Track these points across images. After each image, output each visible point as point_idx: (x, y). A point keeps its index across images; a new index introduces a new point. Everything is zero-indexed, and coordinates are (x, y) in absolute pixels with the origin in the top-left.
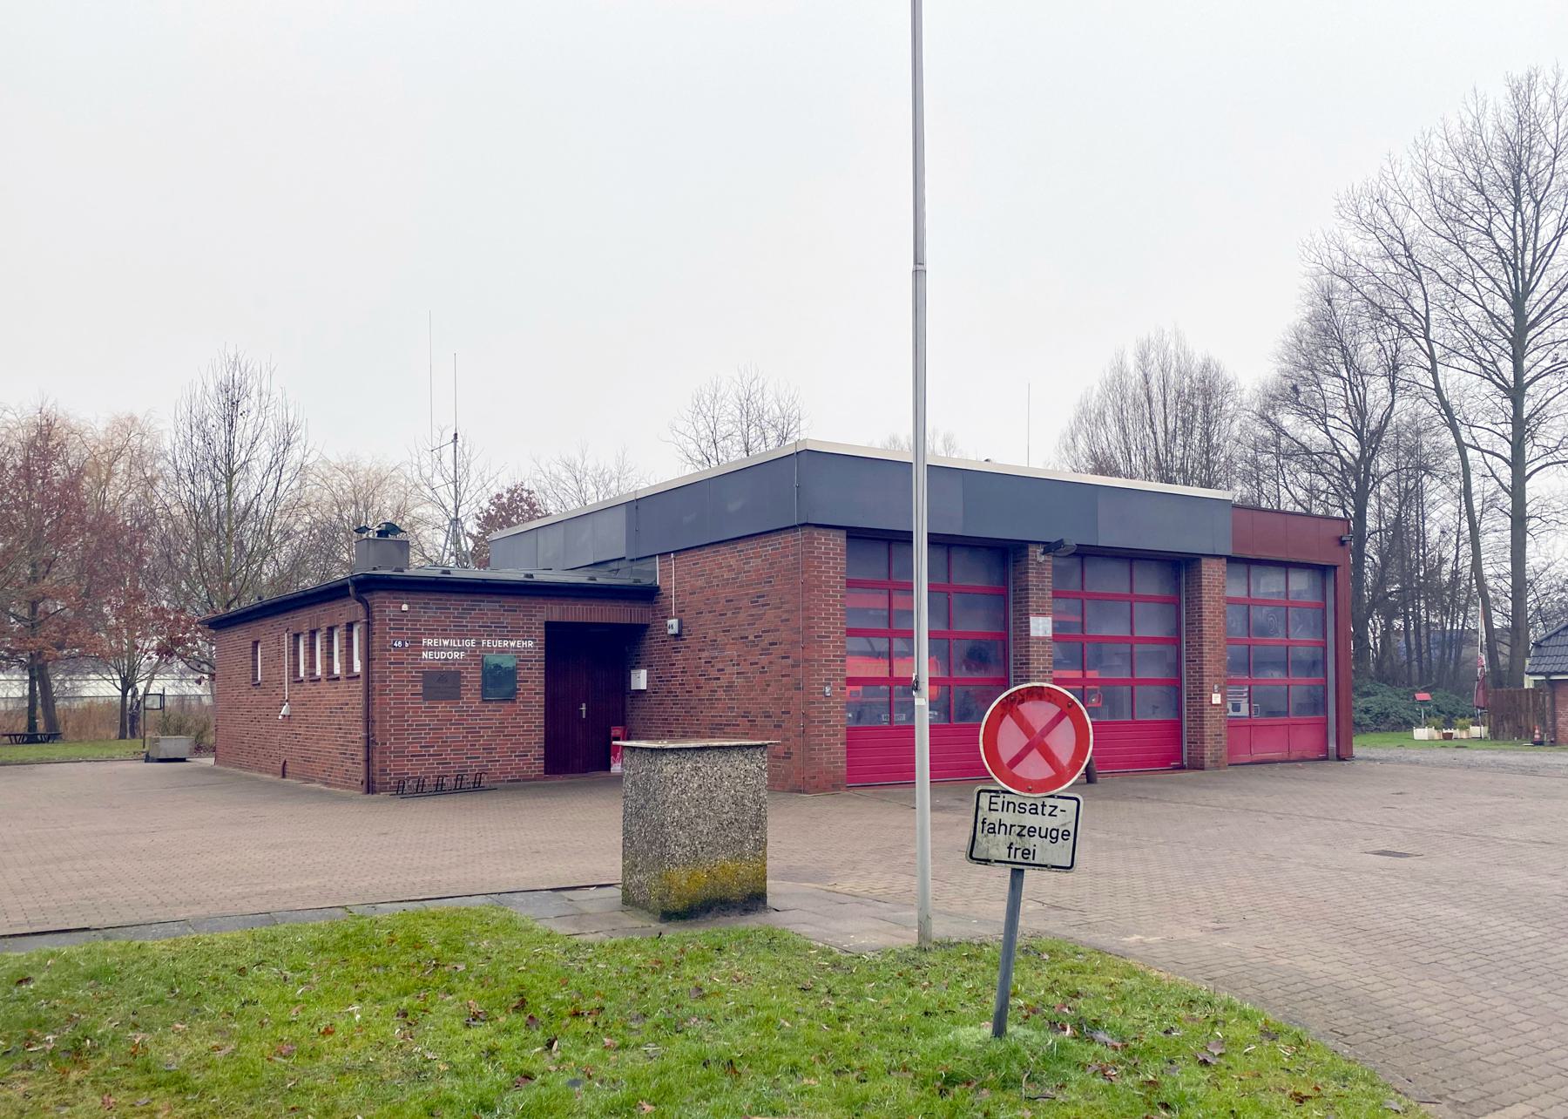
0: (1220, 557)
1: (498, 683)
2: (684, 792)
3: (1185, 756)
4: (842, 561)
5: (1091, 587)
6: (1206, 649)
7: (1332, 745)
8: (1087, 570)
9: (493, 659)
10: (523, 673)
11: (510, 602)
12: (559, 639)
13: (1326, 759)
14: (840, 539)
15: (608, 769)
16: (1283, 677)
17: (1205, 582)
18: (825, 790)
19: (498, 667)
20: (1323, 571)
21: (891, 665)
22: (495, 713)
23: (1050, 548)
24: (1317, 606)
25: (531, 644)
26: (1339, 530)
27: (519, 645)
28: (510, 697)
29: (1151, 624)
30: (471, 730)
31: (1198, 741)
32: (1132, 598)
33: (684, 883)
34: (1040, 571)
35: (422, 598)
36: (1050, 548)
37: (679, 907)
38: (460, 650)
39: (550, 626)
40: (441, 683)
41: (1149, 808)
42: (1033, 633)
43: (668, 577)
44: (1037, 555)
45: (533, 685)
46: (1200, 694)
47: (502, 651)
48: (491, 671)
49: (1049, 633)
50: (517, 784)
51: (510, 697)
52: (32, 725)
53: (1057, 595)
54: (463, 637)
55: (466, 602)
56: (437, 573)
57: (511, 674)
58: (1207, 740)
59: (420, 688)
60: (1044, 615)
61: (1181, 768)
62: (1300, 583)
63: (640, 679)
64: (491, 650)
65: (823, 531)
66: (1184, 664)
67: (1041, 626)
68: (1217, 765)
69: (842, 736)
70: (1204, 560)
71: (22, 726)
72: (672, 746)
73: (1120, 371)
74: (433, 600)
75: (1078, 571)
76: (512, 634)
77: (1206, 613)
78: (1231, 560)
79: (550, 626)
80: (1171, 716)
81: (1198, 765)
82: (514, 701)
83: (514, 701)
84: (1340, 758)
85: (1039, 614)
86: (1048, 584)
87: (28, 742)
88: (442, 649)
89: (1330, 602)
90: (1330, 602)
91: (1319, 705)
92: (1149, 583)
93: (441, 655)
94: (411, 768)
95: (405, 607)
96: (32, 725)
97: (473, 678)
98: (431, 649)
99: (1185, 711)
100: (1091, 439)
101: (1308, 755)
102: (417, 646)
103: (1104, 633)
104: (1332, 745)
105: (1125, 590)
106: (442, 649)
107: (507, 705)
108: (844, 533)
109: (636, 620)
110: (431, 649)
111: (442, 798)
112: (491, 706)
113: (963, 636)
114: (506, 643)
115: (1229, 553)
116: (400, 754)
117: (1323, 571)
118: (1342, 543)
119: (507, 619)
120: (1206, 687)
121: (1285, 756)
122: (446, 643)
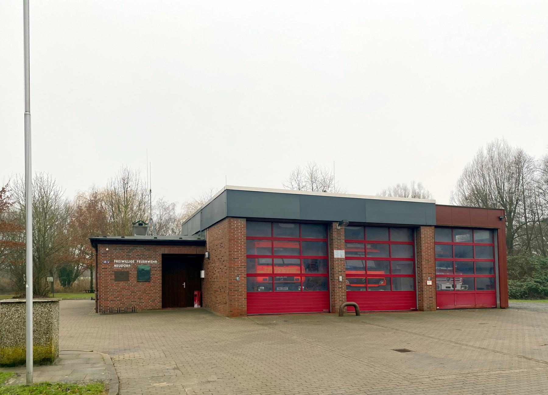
0: (431, 226)
1: (144, 275)
2: (11, 319)
3: (418, 306)
4: (244, 230)
5: (392, 239)
6: (423, 263)
7: (498, 302)
8: (391, 233)
9: (141, 267)
10: (153, 272)
11: (148, 247)
12: (166, 259)
13: (496, 308)
14: (244, 222)
15: (193, 306)
16: (452, 274)
17: (422, 236)
18: (237, 316)
19: (143, 270)
20: (493, 231)
21: (273, 269)
22: (143, 286)
23: (341, 223)
24: (490, 245)
25: (156, 262)
26: (499, 214)
27: (152, 262)
28: (148, 280)
29: (403, 253)
30: (133, 292)
31: (422, 300)
32: (390, 243)
33: (10, 353)
34: (338, 234)
35: (114, 246)
36: (341, 223)
37: (8, 362)
38: (128, 264)
39: (164, 256)
40: (122, 275)
41: (368, 326)
42: (335, 256)
43: (208, 237)
44: (336, 226)
45: (157, 277)
46: (421, 281)
47: (145, 264)
48: (140, 271)
49: (344, 257)
50: (150, 311)
51: (148, 280)
52: (92, 287)
53: (347, 241)
54: (129, 259)
55: (131, 247)
56: (178, 239)
57: (148, 273)
58: (425, 299)
59: (113, 277)
60: (340, 249)
61: (416, 310)
62: (483, 237)
63: (203, 274)
64: (141, 264)
65: (235, 219)
66: (416, 269)
67: (339, 254)
68: (430, 309)
69: (245, 296)
70: (422, 227)
71: (88, 287)
72: (12, 301)
73: (481, 155)
74: (118, 247)
75: (362, 234)
76: (149, 258)
77: (423, 248)
78: (436, 227)
79: (164, 256)
80: (412, 290)
81: (422, 310)
82: (150, 282)
83: (150, 282)
84: (501, 308)
85: (338, 249)
86: (343, 237)
87: (91, 293)
88: (122, 263)
89: (496, 244)
90: (496, 244)
91: (493, 286)
92: (402, 237)
93: (122, 266)
94: (110, 304)
95: (107, 249)
96: (92, 287)
97: (134, 273)
98: (118, 263)
99: (417, 288)
100: (469, 182)
101: (485, 306)
102: (112, 261)
103: (396, 257)
104: (498, 302)
105: (387, 239)
106: (122, 263)
107: (146, 284)
108: (245, 220)
109: (198, 253)
110: (118, 263)
111: (111, 315)
112: (140, 284)
113: (307, 258)
114: (146, 261)
115: (435, 224)
116: (106, 299)
117: (493, 231)
118: (501, 219)
119: (147, 253)
120: (424, 278)
121: (473, 306)
122: (123, 261)
